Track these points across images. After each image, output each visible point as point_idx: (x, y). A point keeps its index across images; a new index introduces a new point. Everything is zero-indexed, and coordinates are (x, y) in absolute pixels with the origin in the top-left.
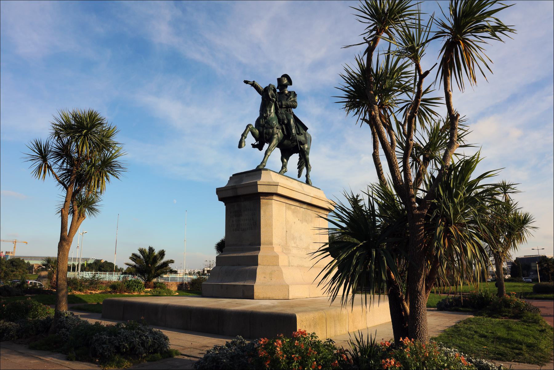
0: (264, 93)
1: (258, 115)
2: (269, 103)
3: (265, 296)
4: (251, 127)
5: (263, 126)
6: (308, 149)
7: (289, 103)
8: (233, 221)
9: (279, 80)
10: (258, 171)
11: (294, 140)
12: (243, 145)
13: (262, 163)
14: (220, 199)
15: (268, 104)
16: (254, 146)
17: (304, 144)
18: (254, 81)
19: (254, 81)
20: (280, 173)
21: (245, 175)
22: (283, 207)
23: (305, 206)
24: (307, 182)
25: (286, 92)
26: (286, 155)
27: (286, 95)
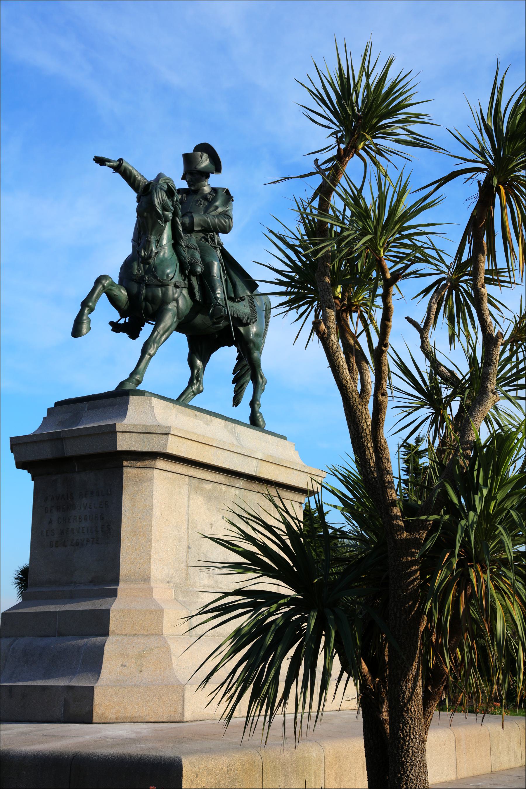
0: (145, 192)
1: (127, 250)
2: (155, 223)
3: (122, 714)
4: (106, 283)
5: (140, 281)
6: (261, 335)
7: (211, 219)
8: (50, 522)
9: (188, 158)
10: (119, 397)
11: (219, 315)
12: (84, 330)
13: (132, 375)
14: (20, 465)
15: (153, 226)
16: (116, 327)
17: (247, 324)
18: (121, 160)
19: (121, 160)
20: (181, 400)
21: (86, 405)
22: (183, 486)
23: (241, 483)
24: (255, 422)
25: (207, 190)
26: (201, 348)
27: (205, 198)
